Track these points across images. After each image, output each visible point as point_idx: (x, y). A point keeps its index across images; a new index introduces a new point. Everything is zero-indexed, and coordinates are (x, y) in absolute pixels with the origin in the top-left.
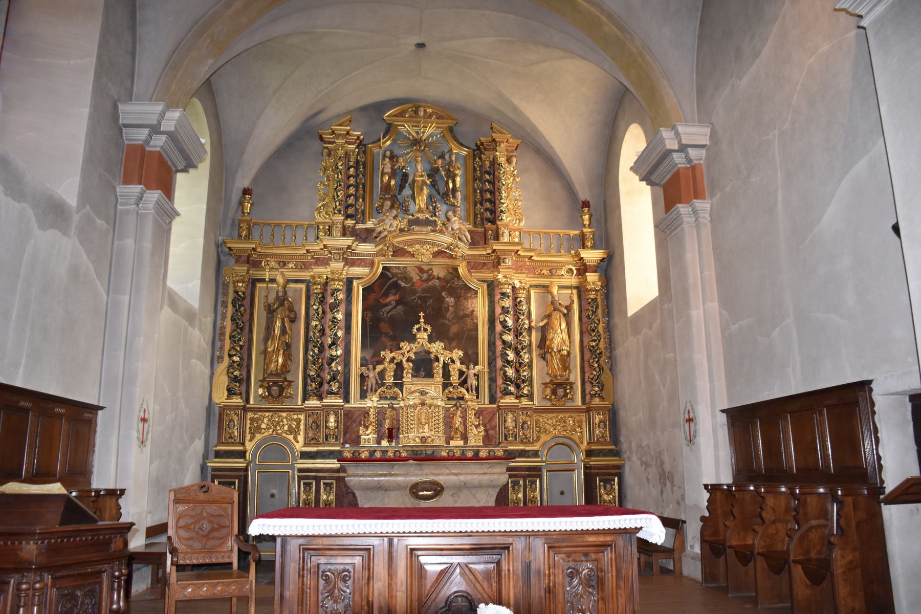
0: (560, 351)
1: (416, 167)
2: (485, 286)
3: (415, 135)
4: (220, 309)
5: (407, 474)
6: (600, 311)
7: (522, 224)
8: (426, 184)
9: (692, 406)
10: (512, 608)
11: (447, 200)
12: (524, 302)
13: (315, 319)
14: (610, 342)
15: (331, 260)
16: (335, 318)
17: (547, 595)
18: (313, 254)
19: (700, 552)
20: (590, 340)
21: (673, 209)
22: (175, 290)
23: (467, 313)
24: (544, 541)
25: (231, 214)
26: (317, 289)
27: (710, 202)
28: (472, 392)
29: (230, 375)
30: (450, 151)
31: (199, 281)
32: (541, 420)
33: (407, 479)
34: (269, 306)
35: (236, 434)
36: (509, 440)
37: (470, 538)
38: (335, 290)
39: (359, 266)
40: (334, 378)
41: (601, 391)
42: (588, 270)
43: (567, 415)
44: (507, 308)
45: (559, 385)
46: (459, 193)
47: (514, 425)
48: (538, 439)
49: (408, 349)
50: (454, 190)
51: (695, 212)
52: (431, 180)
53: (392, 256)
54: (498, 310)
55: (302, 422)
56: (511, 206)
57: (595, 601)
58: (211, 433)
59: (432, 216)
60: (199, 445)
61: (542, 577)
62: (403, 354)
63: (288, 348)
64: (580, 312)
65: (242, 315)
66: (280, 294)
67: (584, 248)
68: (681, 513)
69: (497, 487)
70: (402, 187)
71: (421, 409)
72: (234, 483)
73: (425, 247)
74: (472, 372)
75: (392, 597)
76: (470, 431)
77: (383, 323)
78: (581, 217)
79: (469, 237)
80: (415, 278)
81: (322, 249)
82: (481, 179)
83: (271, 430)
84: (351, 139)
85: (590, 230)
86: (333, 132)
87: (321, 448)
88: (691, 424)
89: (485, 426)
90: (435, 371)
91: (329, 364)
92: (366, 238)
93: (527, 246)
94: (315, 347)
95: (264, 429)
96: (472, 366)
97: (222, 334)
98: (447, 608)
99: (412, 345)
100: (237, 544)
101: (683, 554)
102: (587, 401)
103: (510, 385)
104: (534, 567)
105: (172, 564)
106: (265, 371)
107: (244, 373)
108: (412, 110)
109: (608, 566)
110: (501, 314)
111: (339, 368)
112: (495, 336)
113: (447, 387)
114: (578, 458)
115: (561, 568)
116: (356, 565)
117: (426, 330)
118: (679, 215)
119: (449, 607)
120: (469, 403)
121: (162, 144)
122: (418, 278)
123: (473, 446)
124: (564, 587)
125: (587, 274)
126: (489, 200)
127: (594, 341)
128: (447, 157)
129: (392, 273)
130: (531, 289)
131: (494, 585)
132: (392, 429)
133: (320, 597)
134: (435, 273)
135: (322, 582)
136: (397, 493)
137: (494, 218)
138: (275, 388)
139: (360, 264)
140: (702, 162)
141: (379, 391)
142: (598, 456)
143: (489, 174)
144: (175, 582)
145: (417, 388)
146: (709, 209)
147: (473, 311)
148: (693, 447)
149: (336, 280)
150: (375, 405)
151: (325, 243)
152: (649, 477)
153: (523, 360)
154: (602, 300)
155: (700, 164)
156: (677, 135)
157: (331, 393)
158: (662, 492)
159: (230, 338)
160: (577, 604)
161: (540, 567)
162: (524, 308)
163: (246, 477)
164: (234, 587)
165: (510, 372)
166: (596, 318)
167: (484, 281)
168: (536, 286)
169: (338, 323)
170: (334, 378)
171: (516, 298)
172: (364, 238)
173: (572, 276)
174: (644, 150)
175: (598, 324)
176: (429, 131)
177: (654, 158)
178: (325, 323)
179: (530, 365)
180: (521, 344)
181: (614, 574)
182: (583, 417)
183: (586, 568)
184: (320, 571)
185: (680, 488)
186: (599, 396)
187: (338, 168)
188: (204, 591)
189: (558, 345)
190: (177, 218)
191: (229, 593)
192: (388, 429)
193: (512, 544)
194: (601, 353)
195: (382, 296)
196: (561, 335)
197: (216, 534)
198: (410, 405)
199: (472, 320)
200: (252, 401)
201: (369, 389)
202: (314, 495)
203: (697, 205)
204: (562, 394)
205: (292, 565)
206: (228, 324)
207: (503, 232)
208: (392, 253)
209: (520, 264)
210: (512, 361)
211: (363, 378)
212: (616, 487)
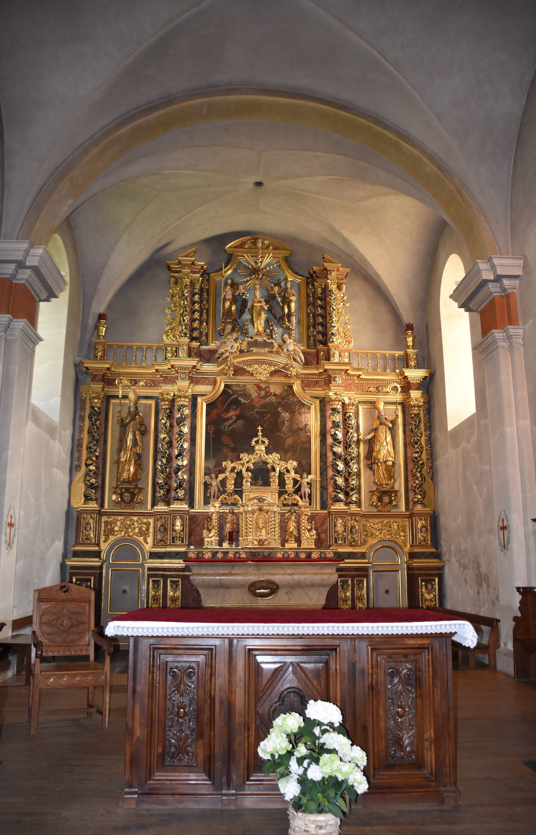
0: (385, 462)
1: (255, 294)
2: (318, 402)
3: (254, 264)
4: (78, 422)
5: (246, 574)
6: (422, 425)
7: (352, 345)
8: (263, 309)
9: (505, 515)
10: (339, 704)
11: (283, 324)
12: (353, 417)
13: (163, 432)
14: (432, 453)
15: (177, 379)
16: (181, 431)
17: (370, 692)
18: (161, 373)
19: (512, 649)
20: (414, 451)
21: (489, 334)
22: (38, 406)
23: (301, 426)
24: (368, 643)
25: (87, 337)
26: (165, 405)
27: (523, 327)
28: (305, 499)
29: (87, 482)
30: (286, 279)
31: (59, 399)
32: (368, 525)
33: (246, 578)
34: (122, 420)
35: (92, 536)
36: (339, 543)
37: (301, 640)
38: (182, 405)
39: (203, 384)
40: (180, 486)
41: (423, 498)
42: (412, 387)
43: (392, 520)
44: (338, 422)
45: (385, 493)
46: (294, 317)
47: (343, 530)
48: (365, 542)
49: (247, 460)
50: (289, 315)
51: (509, 337)
52: (268, 306)
53: (233, 375)
54: (329, 424)
55: (152, 525)
56: (341, 329)
57: (413, 698)
58: (70, 534)
59: (269, 339)
60: (59, 545)
61: (366, 676)
62: (243, 465)
63: (139, 460)
64: (404, 426)
65: (98, 428)
66: (132, 409)
67: (407, 367)
68: (495, 612)
69: (327, 586)
70: (241, 312)
71: (259, 515)
72: (90, 580)
73: (263, 367)
74: (305, 481)
75: (232, 692)
76: (303, 535)
77: (224, 436)
78: (406, 339)
79: (303, 358)
80: (254, 394)
81: (169, 369)
82: (314, 304)
83: (123, 533)
84: (196, 269)
85: (414, 351)
86: (180, 263)
87: (168, 549)
88: (505, 532)
89: (316, 530)
90: (271, 480)
91: (176, 473)
92: (209, 359)
93: (355, 365)
94: (163, 457)
95: (117, 531)
96: (305, 475)
97: (80, 445)
98: (281, 702)
99: (251, 456)
100: (94, 638)
101: (497, 650)
102: (410, 507)
103: (340, 493)
104: (358, 666)
105: (37, 656)
106: (118, 479)
107: (100, 480)
108: (251, 242)
109: (425, 667)
110: (331, 428)
111: (185, 477)
112: (326, 448)
113: (282, 494)
114: (402, 560)
115: (383, 668)
116: (200, 662)
117: (263, 442)
118: (495, 341)
119: (282, 702)
120: (303, 509)
121: (26, 277)
122: (257, 395)
123: (306, 549)
124: (385, 685)
125: (411, 391)
126: (321, 324)
127: (417, 452)
128: (283, 284)
129: (233, 391)
130: (359, 405)
131: (323, 682)
132: (232, 532)
133: (168, 691)
134: (272, 391)
135: (169, 678)
136: (237, 591)
137: (326, 340)
138: (127, 494)
139: (204, 382)
140: (515, 291)
141: (221, 497)
142: (420, 558)
143: (321, 300)
144: (39, 673)
145: (255, 495)
146: (522, 334)
147: (306, 425)
148: (507, 553)
149: (183, 397)
150: (217, 510)
151: (172, 363)
152: (467, 578)
153: (352, 470)
154: (424, 415)
155: (514, 293)
156: (493, 267)
157: (178, 499)
158: (478, 592)
159: (87, 449)
160: (397, 701)
161: (364, 667)
162: (353, 422)
163: (101, 574)
164: (91, 678)
165: (340, 481)
166: (419, 432)
167: (316, 398)
168: (364, 402)
169: (184, 436)
170: (180, 486)
171: (346, 413)
172: (207, 358)
173: (397, 393)
174: (463, 280)
175: (420, 437)
176: (266, 261)
177: (472, 288)
178: (173, 436)
179: (358, 475)
180: (350, 455)
181: (431, 674)
182: (407, 522)
183: (405, 669)
184: (168, 667)
185: (495, 589)
186: (421, 503)
187: (184, 295)
188: (64, 681)
189: (384, 456)
190: (41, 343)
191: (87, 683)
192: (229, 532)
193: (339, 646)
194: (423, 464)
195: (223, 412)
196: (386, 448)
197: (75, 629)
198: (249, 511)
199: (306, 433)
200: (106, 506)
201: (212, 496)
202: (161, 591)
203: (511, 330)
204: (388, 501)
205: (143, 662)
206: (85, 437)
207: (334, 353)
208: (233, 373)
209: (349, 382)
210: (342, 471)
211: (207, 486)
212: (437, 587)
